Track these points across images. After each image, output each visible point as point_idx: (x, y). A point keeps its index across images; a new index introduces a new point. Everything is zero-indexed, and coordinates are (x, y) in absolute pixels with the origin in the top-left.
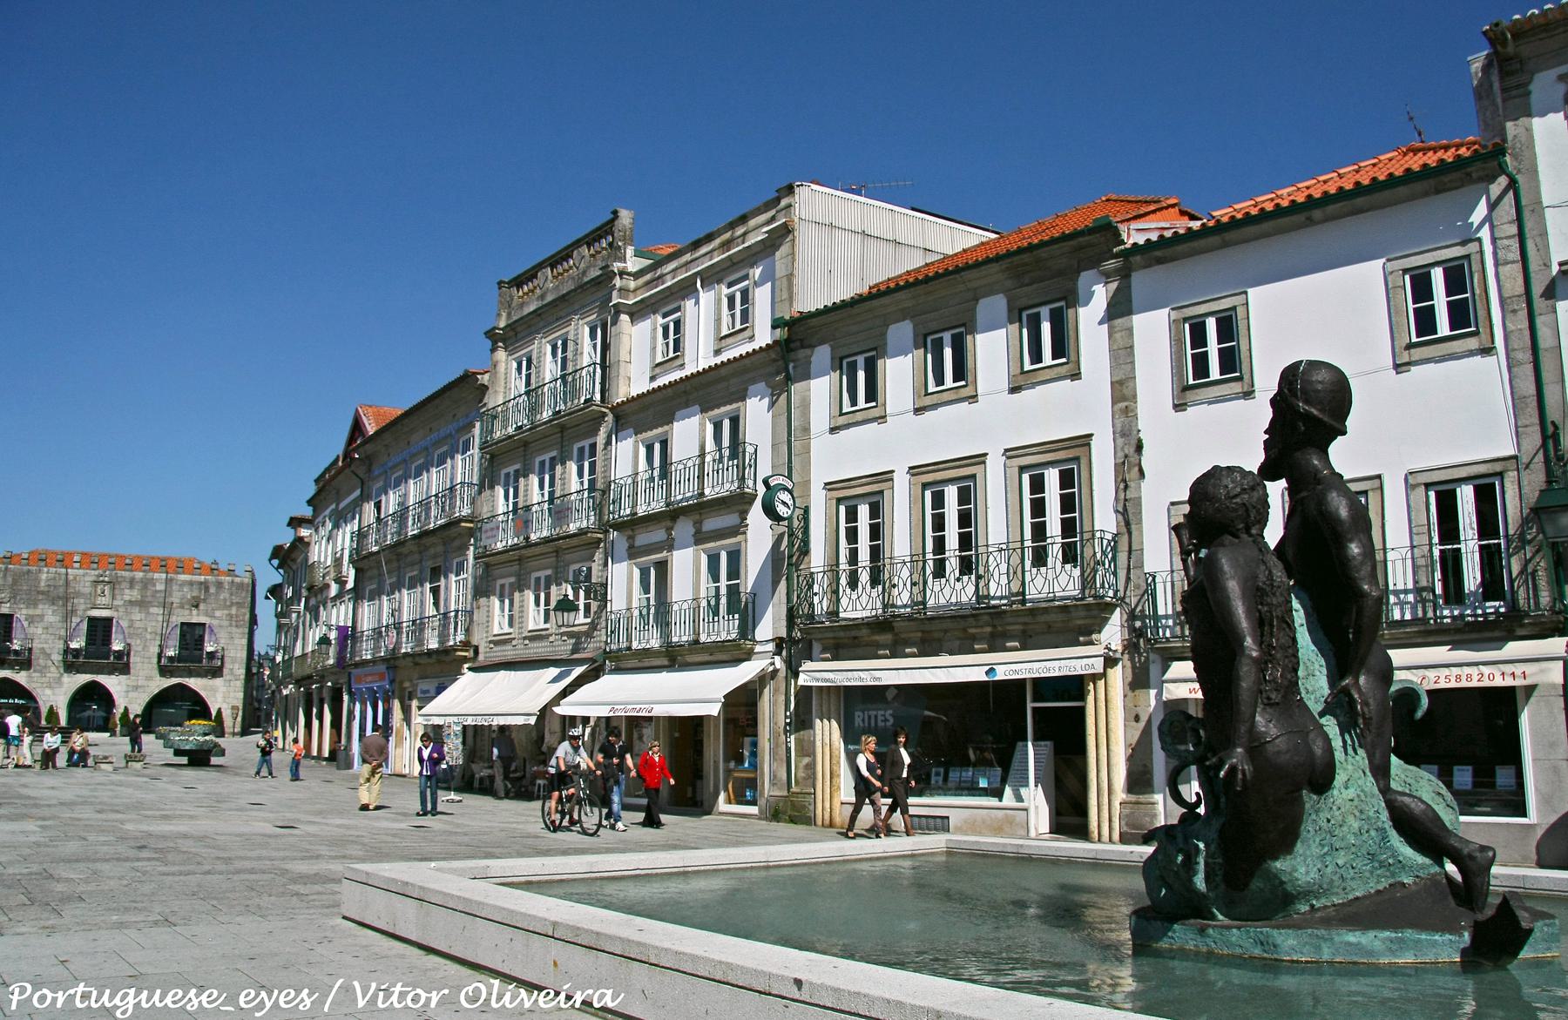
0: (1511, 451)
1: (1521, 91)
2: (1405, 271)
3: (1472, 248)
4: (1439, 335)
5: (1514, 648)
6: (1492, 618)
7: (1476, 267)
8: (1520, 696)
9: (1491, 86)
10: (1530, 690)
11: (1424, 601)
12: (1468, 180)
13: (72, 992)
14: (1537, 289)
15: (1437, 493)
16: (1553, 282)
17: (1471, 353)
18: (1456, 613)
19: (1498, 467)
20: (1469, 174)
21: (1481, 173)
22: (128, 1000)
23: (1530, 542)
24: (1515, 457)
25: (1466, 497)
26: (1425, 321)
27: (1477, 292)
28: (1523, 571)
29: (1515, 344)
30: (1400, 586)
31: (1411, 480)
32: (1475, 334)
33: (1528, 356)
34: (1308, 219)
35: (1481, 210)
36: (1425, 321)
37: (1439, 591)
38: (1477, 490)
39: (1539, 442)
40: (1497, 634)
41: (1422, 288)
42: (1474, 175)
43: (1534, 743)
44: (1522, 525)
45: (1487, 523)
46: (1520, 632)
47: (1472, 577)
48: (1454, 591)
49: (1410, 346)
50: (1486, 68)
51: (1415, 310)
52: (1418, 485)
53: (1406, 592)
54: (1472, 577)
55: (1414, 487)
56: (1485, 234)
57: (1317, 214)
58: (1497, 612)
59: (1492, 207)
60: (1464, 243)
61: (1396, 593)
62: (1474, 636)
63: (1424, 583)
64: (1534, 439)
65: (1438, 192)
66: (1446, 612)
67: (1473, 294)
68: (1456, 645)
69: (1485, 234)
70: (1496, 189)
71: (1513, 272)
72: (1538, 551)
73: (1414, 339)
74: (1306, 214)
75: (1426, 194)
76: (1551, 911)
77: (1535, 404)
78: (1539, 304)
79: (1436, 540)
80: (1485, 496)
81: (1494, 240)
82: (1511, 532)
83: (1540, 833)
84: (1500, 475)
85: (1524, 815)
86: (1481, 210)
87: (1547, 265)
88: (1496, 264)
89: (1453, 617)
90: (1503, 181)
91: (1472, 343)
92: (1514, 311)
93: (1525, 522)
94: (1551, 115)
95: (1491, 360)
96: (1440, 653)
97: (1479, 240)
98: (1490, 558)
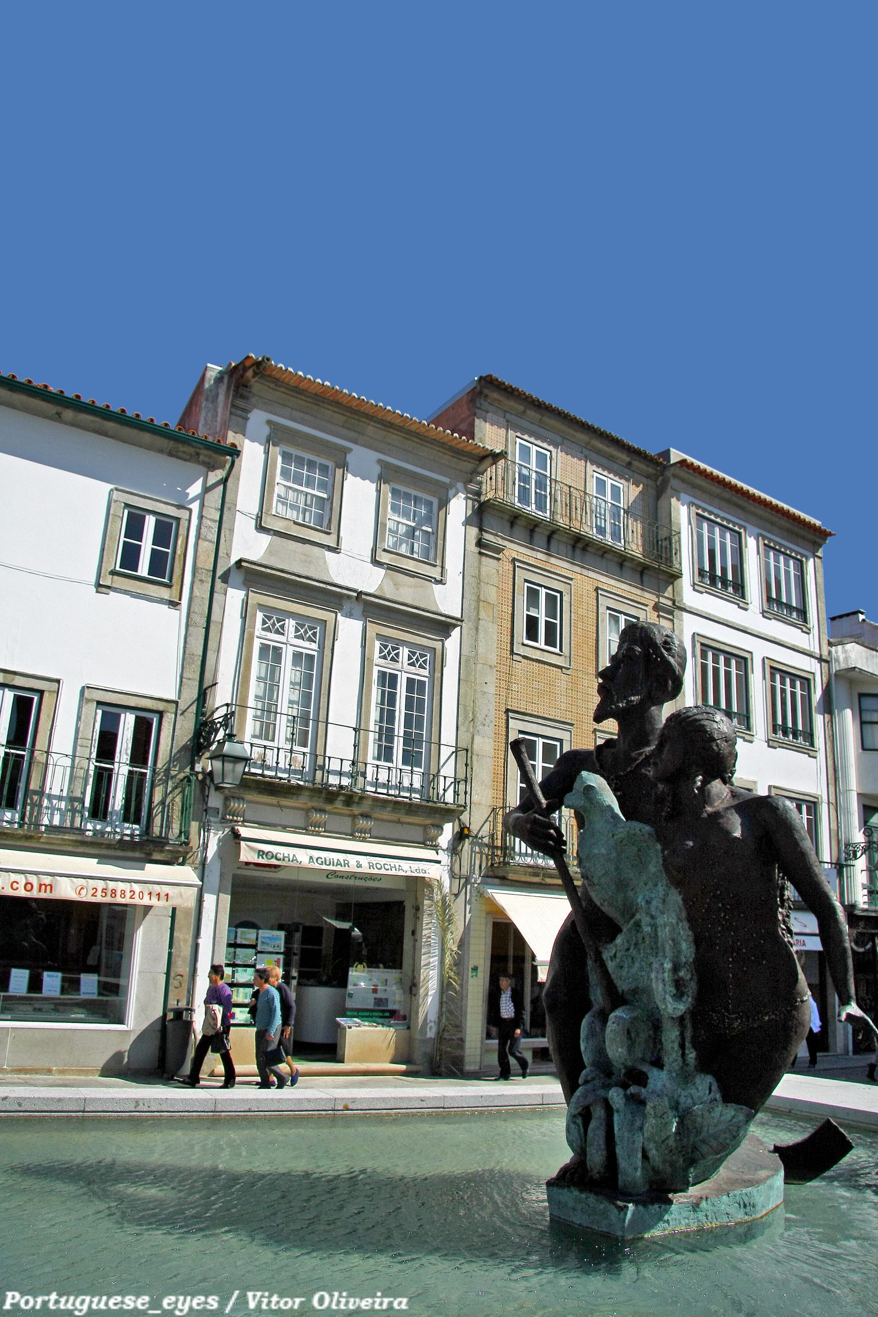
0: (173, 696)
1: (244, 414)
2: (127, 505)
3: (183, 514)
4: (139, 573)
5: (153, 871)
6: (128, 838)
7: (182, 531)
8: (139, 912)
9: (217, 396)
10: (148, 909)
11: (74, 811)
12: (194, 458)
13: (46, 1298)
14: (219, 573)
15: (104, 713)
16: (229, 570)
17: (161, 601)
18: (98, 827)
19: (160, 706)
20: (198, 454)
21: (207, 460)
22: (81, 1304)
23: (173, 777)
24: (176, 703)
25: (127, 724)
26: (130, 557)
27: (179, 552)
28: (163, 803)
29: (195, 608)
30: (56, 791)
31: (87, 692)
32: (169, 586)
33: (203, 622)
34: (59, 414)
35: (195, 489)
36: (130, 557)
37: (87, 804)
38: (138, 720)
39: (195, 696)
40: (137, 855)
41: (135, 528)
42: (202, 458)
43: (143, 957)
44: (169, 762)
45: (139, 754)
46: (156, 856)
47: (117, 800)
48: (99, 810)
49: (113, 573)
50: (219, 380)
51: (125, 542)
52: (91, 700)
53: (60, 798)
54: (117, 800)
55: (89, 701)
56: (195, 507)
57: (68, 414)
58: (132, 835)
59: (206, 490)
60: (180, 507)
61: (50, 797)
62: (119, 853)
63: (78, 794)
64: (191, 693)
65: (170, 454)
66: (90, 826)
67: (174, 552)
68: (103, 859)
69: (195, 507)
70: (215, 476)
71: (208, 547)
72: (176, 787)
73: (118, 568)
74: (59, 409)
75: (161, 451)
76: (792, 1058)
77: (199, 663)
78: (219, 584)
79: (94, 755)
80: (143, 729)
81: (201, 517)
82: (159, 765)
83: (133, 1037)
84: (161, 714)
85: (121, 1021)
86: (195, 489)
87: (228, 555)
88: (198, 537)
89: (95, 831)
90: (219, 474)
91: (165, 593)
92: (202, 581)
93: (171, 760)
94: (256, 444)
95: (174, 612)
96: (89, 865)
97: (190, 511)
98: (135, 784)
